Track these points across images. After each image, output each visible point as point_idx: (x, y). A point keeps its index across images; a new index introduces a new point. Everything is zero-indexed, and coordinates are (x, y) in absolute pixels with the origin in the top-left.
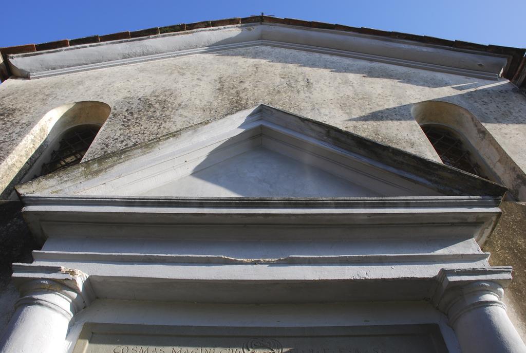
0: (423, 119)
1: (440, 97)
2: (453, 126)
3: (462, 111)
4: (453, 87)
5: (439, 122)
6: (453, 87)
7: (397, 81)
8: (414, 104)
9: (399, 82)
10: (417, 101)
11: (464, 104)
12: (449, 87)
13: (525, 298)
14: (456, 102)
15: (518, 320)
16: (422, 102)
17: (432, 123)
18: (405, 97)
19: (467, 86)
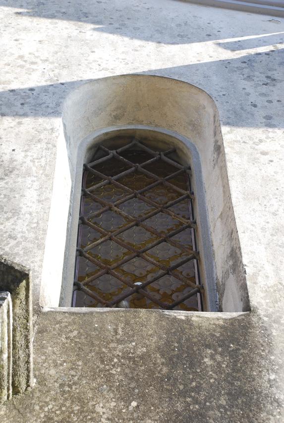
0: (117, 118)
1: (169, 65)
2: (182, 134)
3: (204, 101)
4: (219, 44)
5: (156, 126)
6: (219, 44)
7: (92, 26)
8: (91, 81)
9: (95, 29)
10: (101, 75)
11: (215, 84)
12: (210, 43)
13: (82, 422)
14: (195, 80)
15: (19, 265)
16: (114, 78)
17: (140, 127)
18: (192, 22)
19: (259, 40)
